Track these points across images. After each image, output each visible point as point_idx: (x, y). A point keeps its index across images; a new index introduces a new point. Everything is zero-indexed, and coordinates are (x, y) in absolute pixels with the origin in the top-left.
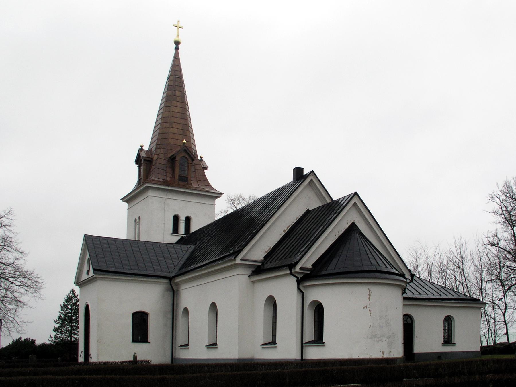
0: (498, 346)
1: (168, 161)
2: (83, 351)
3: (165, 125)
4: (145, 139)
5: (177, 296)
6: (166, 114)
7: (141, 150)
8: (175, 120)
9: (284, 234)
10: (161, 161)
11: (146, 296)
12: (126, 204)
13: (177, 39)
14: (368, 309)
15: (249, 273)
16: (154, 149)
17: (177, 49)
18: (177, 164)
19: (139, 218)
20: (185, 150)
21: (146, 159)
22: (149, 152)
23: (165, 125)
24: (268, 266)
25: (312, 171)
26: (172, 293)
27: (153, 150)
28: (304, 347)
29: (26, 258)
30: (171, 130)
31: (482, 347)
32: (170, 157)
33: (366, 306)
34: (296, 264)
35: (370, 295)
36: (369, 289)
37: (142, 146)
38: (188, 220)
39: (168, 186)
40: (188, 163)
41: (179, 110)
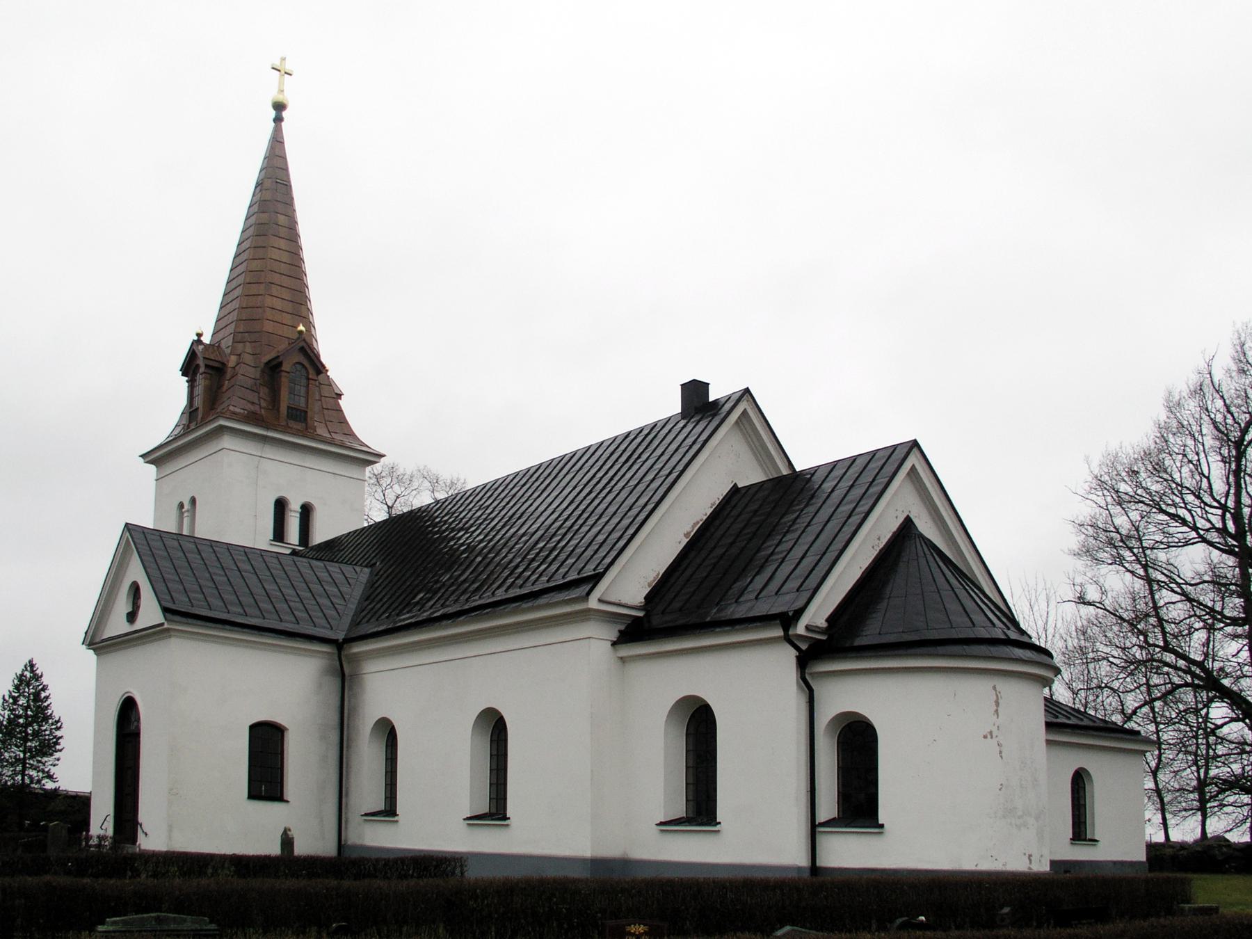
0: (1210, 847)
1: (263, 371)
2: (112, 814)
3: (254, 289)
4: (199, 315)
5: (351, 688)
6: (255, 265)
7: (198, 342)
8: (276, 278)
9: (685, 541)
10: (246, 371)
11: (282, 682)
12: (153, 468)
13: (280, 98)
14: (995, 740)
15: (614, 636)
16: (227, 343)
17: (278, 120)
18: (284, 380)
19: (193, 501)
20: (302, 350)
21: (211, 363)
22: (214, 346)
23: (254, 289)
24: (657, 621)
25: (747, 391)
26: (338, 681)
27: (223, 345)
28: (819, 838)
30: (269, 301)
31: (1151, 847)
33: (991, 733)
34: (799, 613)
35: (997, 703)
36: (994, 688)
37: (199, 335)
38: (306, 511)
39: (268, 428)
40: (308, 379)
41: (285, 257)
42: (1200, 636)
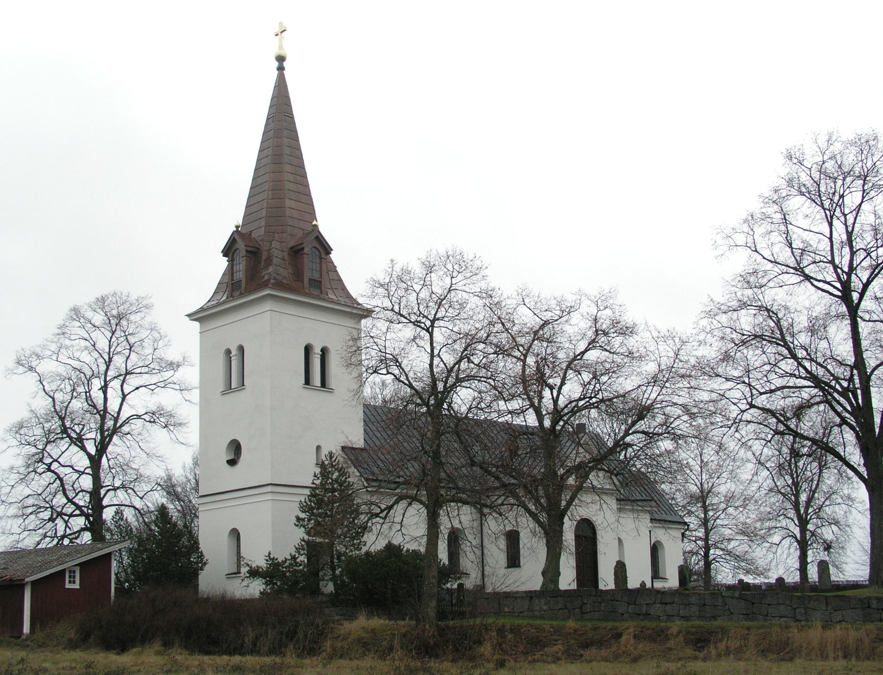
4: (231, 214)
12: (197, 324)
13: (282, 53)
17: (281, 69)
18: (306, 260)
19: (241, 349)
21: (249, 249)
29: (418, 270)
32: (292, 248)
42: (715, 322)
